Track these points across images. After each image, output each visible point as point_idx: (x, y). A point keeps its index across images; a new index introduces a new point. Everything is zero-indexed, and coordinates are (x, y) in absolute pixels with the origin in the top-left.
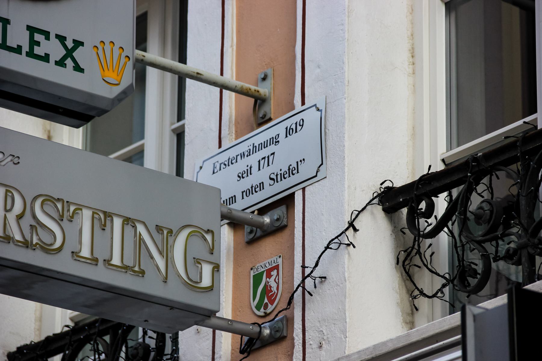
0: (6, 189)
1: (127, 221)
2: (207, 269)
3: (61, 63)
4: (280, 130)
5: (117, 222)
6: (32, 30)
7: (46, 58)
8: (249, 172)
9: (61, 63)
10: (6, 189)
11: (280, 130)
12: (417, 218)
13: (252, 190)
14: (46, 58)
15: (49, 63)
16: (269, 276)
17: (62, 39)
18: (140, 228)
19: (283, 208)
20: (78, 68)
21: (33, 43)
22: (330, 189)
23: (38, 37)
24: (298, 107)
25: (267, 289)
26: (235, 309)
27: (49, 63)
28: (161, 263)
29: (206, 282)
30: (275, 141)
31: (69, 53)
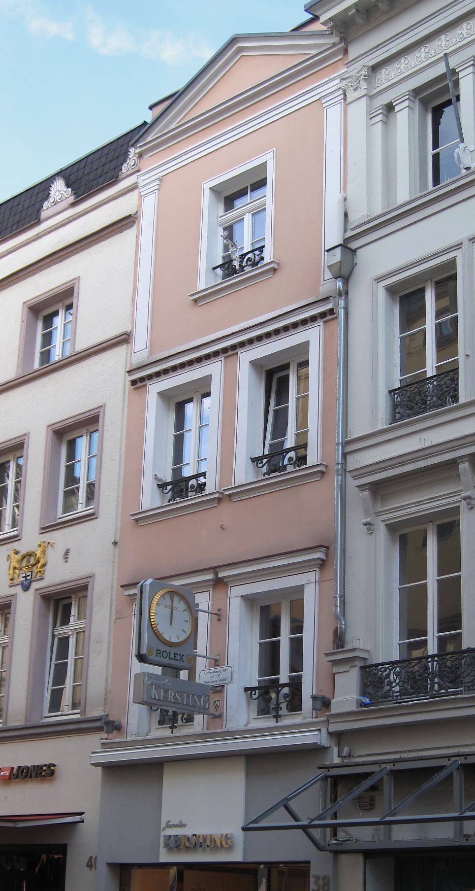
0: (385, 524)
1: (193, 695)
2: (207, 704)
3: (180, 661)
4: (222, 669)
5: (191, 695)
6: (175, 654)
7: (177, 660)
8: (213, 677)
9: (180, 661)
10: (385, 524)
11: (222, 669)
12: (430, 684)
13: (214, 681)
14: (177, 660)
15: (309, 341)
16: (218, 702)
17: (180, 655)
18: (195, 697)
19: (221, 688)
20: (183, 661)
21: (175, 657)
22: (424, 666)
23: (176, 655)
24: (226, 665)
25: (217, 705)
26: (378, 817)
27: (309, 341)
28: (199, 704)
29: (207, 707)
30: (220, 672)
31: (181, 658)
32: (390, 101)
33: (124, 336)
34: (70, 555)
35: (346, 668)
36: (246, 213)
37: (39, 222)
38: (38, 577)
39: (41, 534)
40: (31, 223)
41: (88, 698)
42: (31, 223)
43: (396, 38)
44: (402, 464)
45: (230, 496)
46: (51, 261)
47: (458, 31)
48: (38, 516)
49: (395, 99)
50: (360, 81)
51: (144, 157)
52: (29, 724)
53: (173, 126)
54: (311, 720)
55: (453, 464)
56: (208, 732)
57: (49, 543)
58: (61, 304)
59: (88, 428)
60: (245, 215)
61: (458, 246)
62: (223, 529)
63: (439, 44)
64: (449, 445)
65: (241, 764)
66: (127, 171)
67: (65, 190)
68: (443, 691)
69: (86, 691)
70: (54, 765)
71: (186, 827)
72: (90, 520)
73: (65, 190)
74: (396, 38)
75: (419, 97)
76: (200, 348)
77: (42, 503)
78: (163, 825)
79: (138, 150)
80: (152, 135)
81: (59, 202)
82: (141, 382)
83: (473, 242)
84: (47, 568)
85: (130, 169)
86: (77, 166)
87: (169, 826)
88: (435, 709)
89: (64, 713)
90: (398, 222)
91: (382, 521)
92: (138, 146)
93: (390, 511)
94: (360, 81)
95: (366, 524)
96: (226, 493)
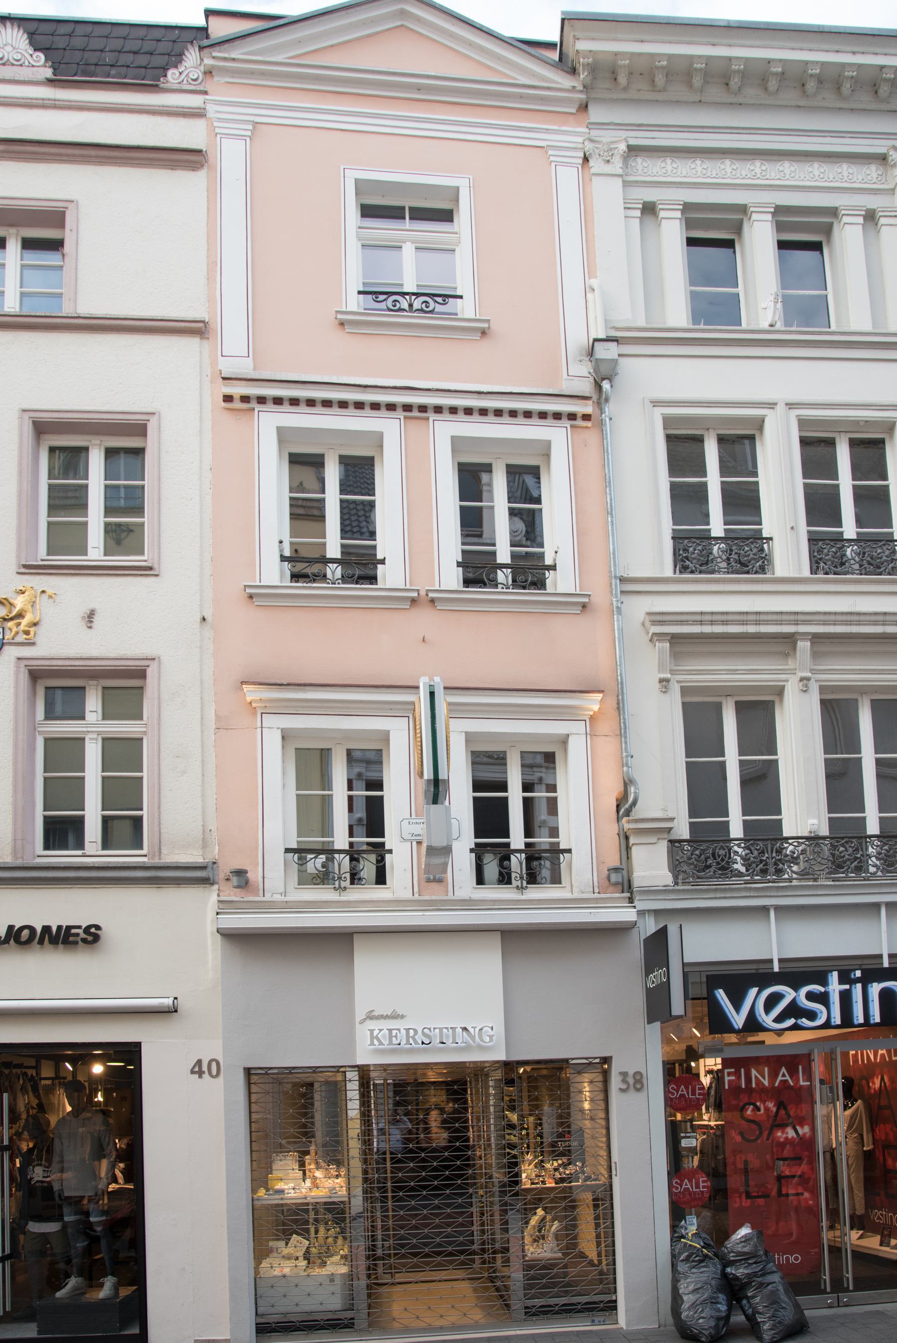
32: (655, 200)
33: (201, 325)
34: (96, 619)
35: (654, 840)
36: (409, 241)
37: (154, 88)
38: (21, 638)
39: (18, 573)
40: (124, 80)
41: (164, 836)
42: (124, 80)
43: (691, 130)
44: (725, 623)
45: (432, 601)
46: (97, 157)
47: (749, 166)
48: (13, 545)
49: (663, 202)
50: (613, 155)
51: (216, 79)
52: (19, 862)
53: (280, 58)
54: (592, 896)
55: (791, 640)
56: (421, 898)
57: (43, 592)
58: (13, 231)
59: (104, 438)
60: (405, 242)
61: (772, 405)
62: (424, 641)
63: (839, 171)
64: (873, 618)
65: (497, 939)
66: (180, 83)
67: (31, 52)
68: (853, 875)
69: (160, 824)
70: (98, 927)
71: (405, 1019)
72: (141, 575)
73: (31, 52)
74: (691, 130)
75: (780, 219)
76: (368, 389)
77: (19, 527)
78: (360, 1014)
79: (208, 61)
80: (241, 51)
81: (13, 65)
82: (420, 411)
83: (790, 408)
84: (42, 630)
85: (185, 82)
86: (52, 26)
87: (370, 1017)
88: (768, 894)
89: (88, 854)
90: (828, 349)
91: (677, 682)
92: (215, 54)
93: (690, 672)
94: (613, 155)
95: (661, 681)
96: (431, 595)
